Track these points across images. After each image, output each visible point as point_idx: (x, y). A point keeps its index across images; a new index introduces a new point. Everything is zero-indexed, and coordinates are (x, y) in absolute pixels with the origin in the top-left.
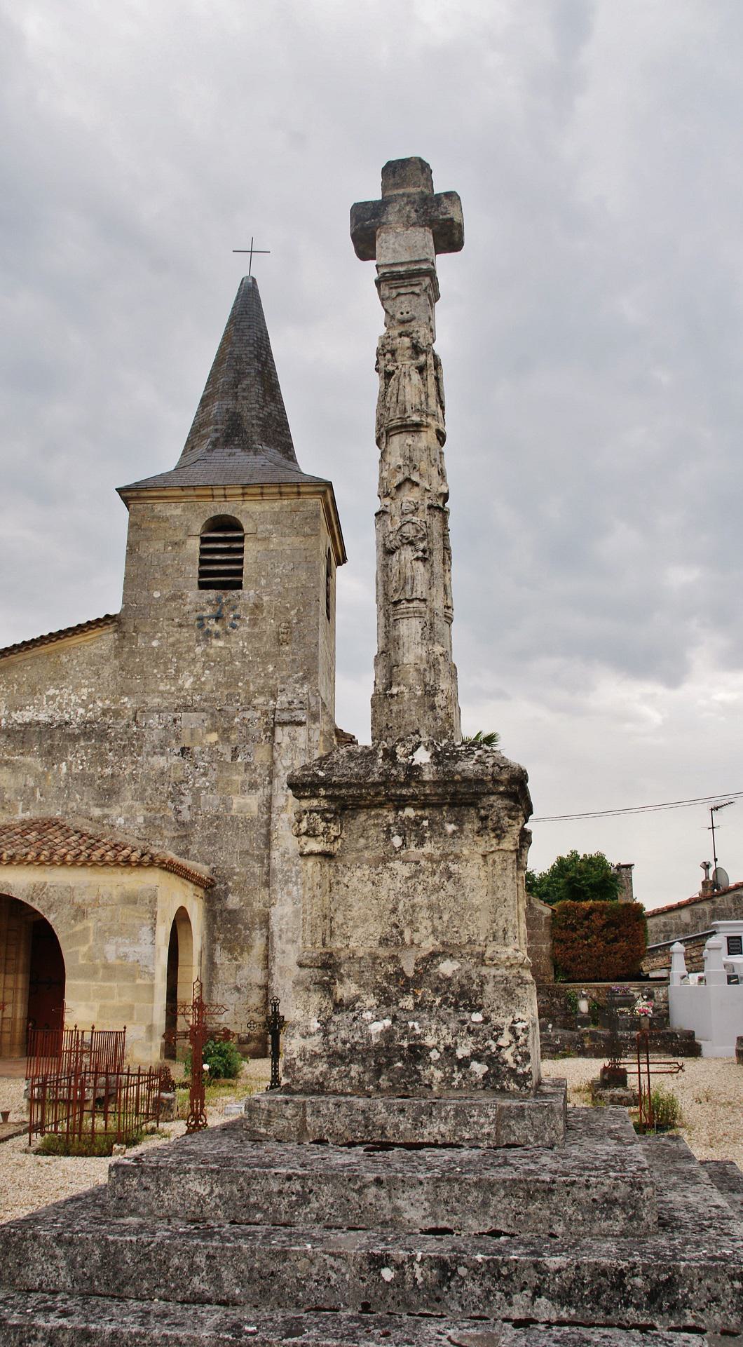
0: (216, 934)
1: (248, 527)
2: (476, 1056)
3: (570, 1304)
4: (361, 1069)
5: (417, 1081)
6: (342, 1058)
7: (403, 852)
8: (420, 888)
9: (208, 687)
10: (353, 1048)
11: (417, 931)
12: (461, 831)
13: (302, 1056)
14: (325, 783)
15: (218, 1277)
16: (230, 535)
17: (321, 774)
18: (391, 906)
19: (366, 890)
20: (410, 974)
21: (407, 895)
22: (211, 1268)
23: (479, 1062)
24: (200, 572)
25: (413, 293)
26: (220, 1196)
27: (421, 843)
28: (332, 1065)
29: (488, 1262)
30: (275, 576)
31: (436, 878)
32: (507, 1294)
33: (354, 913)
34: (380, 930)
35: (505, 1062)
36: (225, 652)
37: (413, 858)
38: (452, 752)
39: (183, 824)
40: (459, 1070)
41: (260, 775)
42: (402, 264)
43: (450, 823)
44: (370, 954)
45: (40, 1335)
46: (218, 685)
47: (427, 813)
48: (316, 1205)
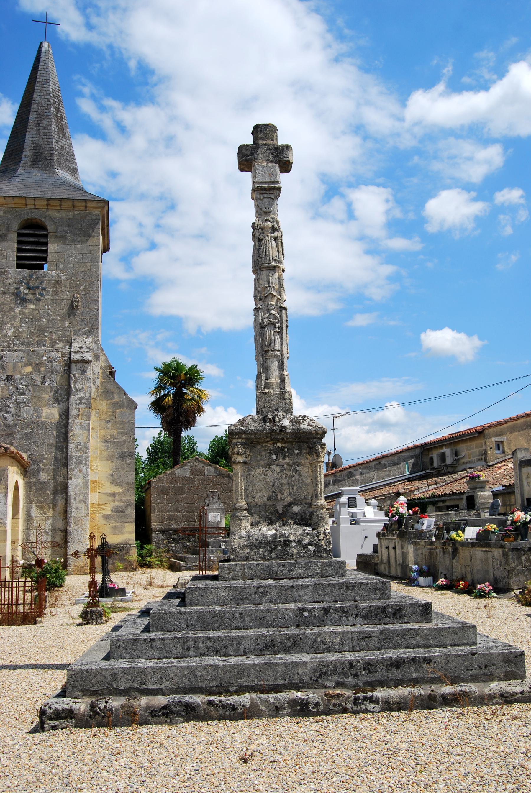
0: (32, 498)
1: (50, 227)
2: (310, 544)
3: (368, 618)
4: (264, 550)
5: (287, 554)
6: (256, 546)
7: (277, 462)
8: (284, 476)
9: (24, 335)
10: (260, 542)
11: (283, 494)
12: (301, 453)
13: (239, 547)
14: (245, 432)
15: (244, 620)
16: (38, 232)
17: (243, 429)
18: (272, 484)
19: (261, 477)
20: (281, 512)
21: (278, 479)
22: (241, 618)
23: (311, 546)
24: (17, 257)
25: (271, 198)
26: (232, 596)
27: (284, 458)
28: (252, 550)
29: (340, 607)
30: (70, 262)
31: (291, 473)
32: (347, 617)
33: (257, 487)
34: (267, 494)
35: (322, 546)
36: (36, 312)
37: (281, 464)
38: (297, 420)
39: (8, 426)
40: (304, 549)
41: (61, 394)
42: (266, 183)
43: (296, 450)
44: (264, 504)
45: (190, 640)
46: (31, 334)
47: (286, 445)
48: (270, 596)
